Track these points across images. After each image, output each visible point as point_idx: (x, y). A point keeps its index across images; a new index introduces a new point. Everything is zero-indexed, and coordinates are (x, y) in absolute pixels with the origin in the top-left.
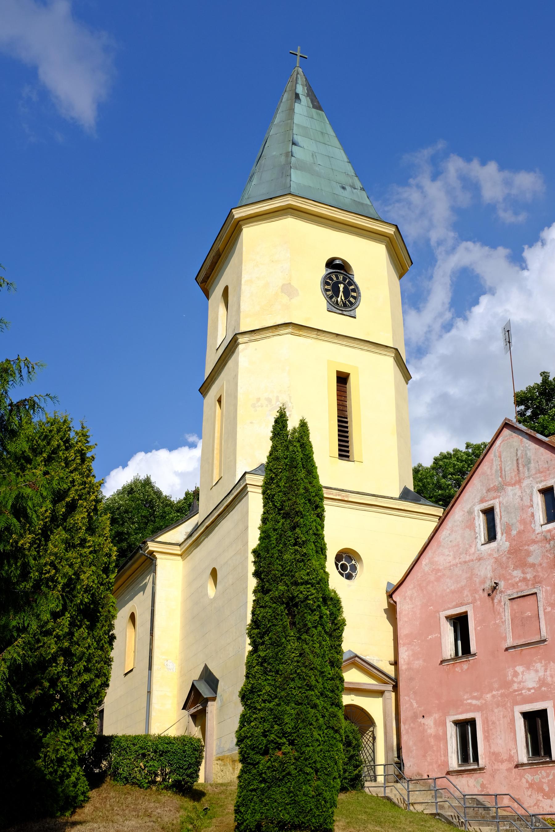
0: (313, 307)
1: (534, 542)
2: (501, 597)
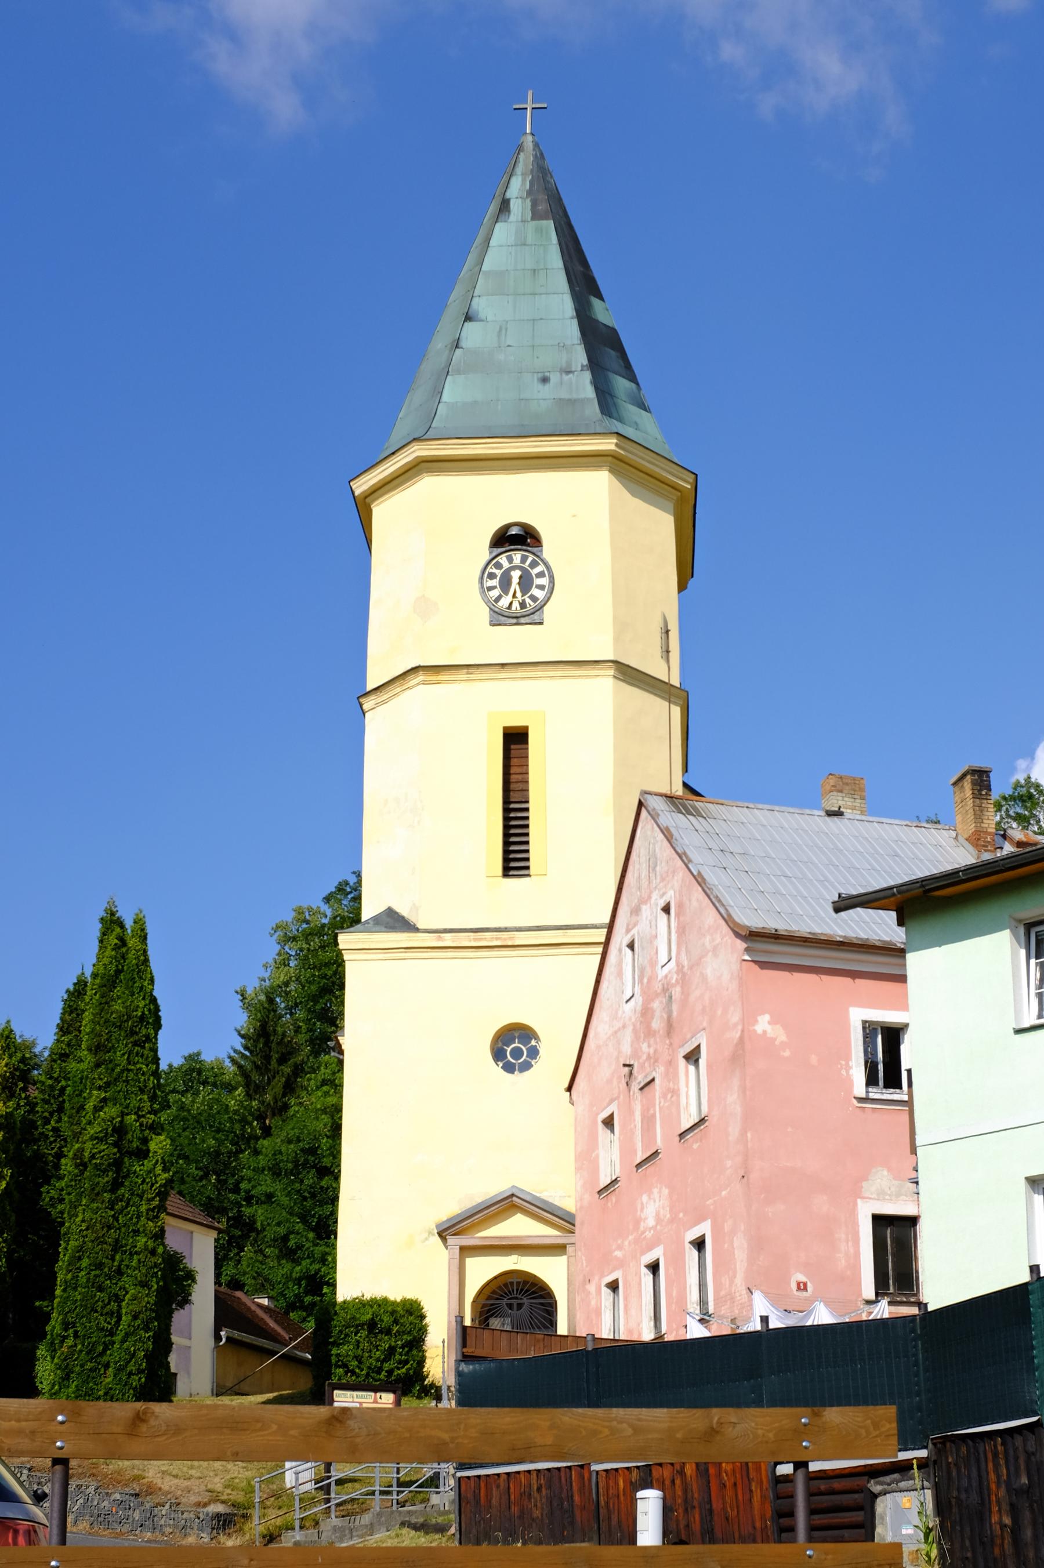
0: (466, 629)
1: (657, 995)
2: (635, 1086)
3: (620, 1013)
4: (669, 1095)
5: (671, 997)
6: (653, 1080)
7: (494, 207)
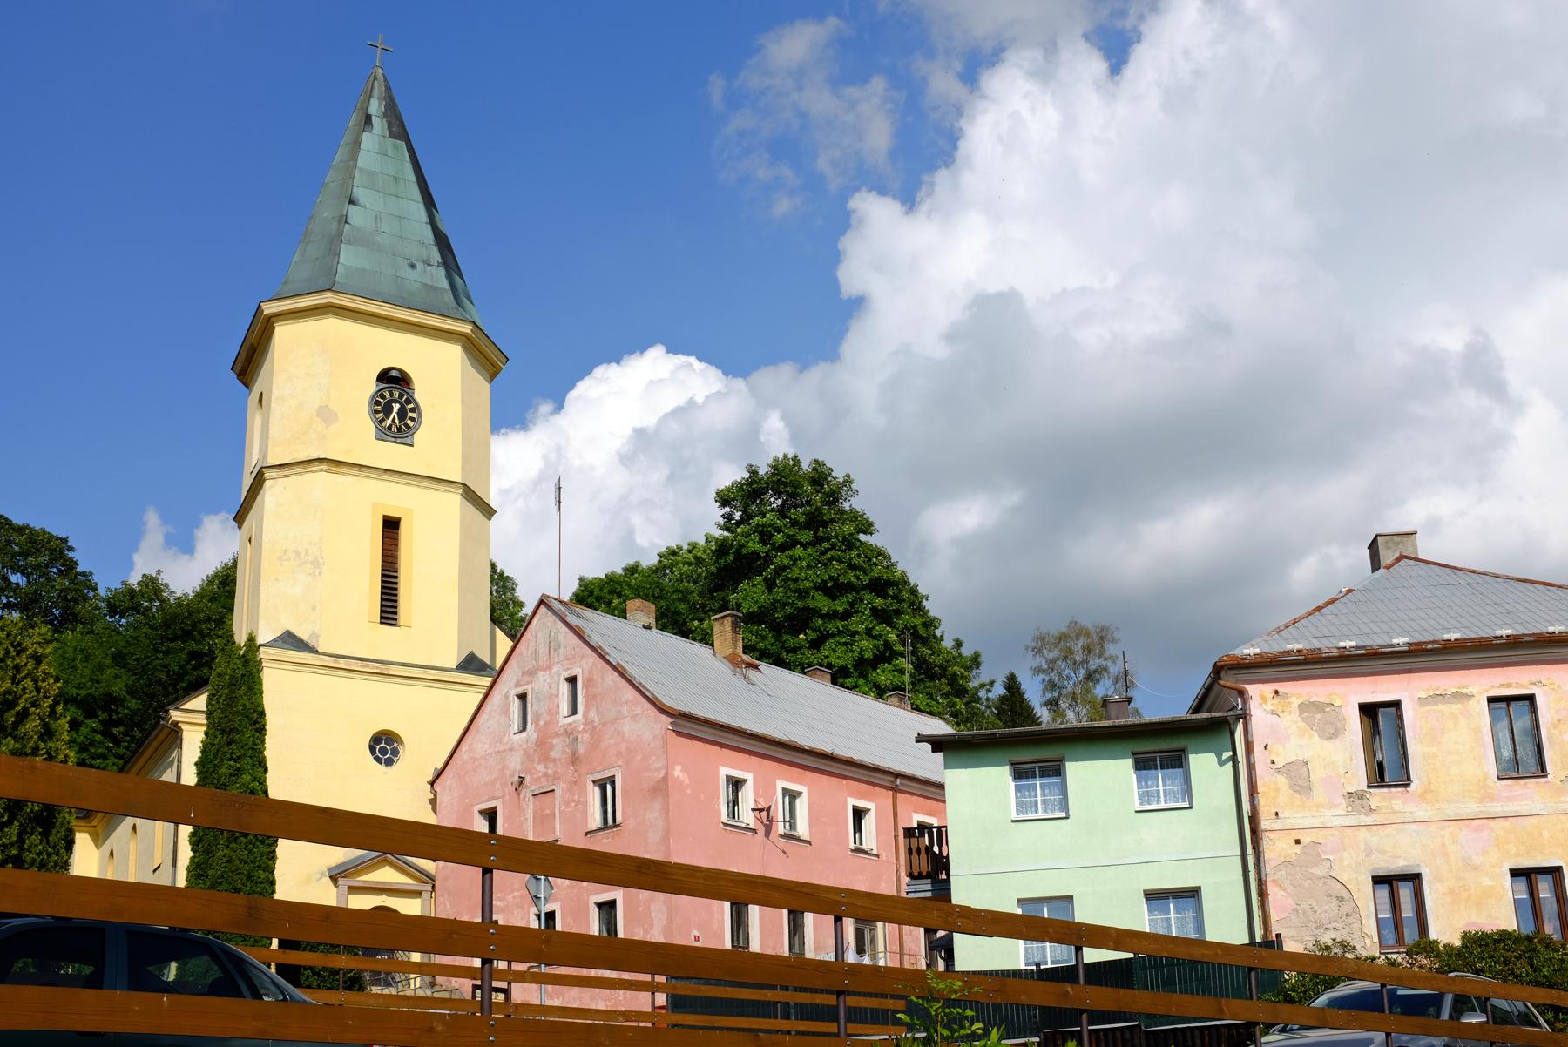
0: (356, 434)
1: (557, 735)
2: (526, 793)
7: (354, 118)
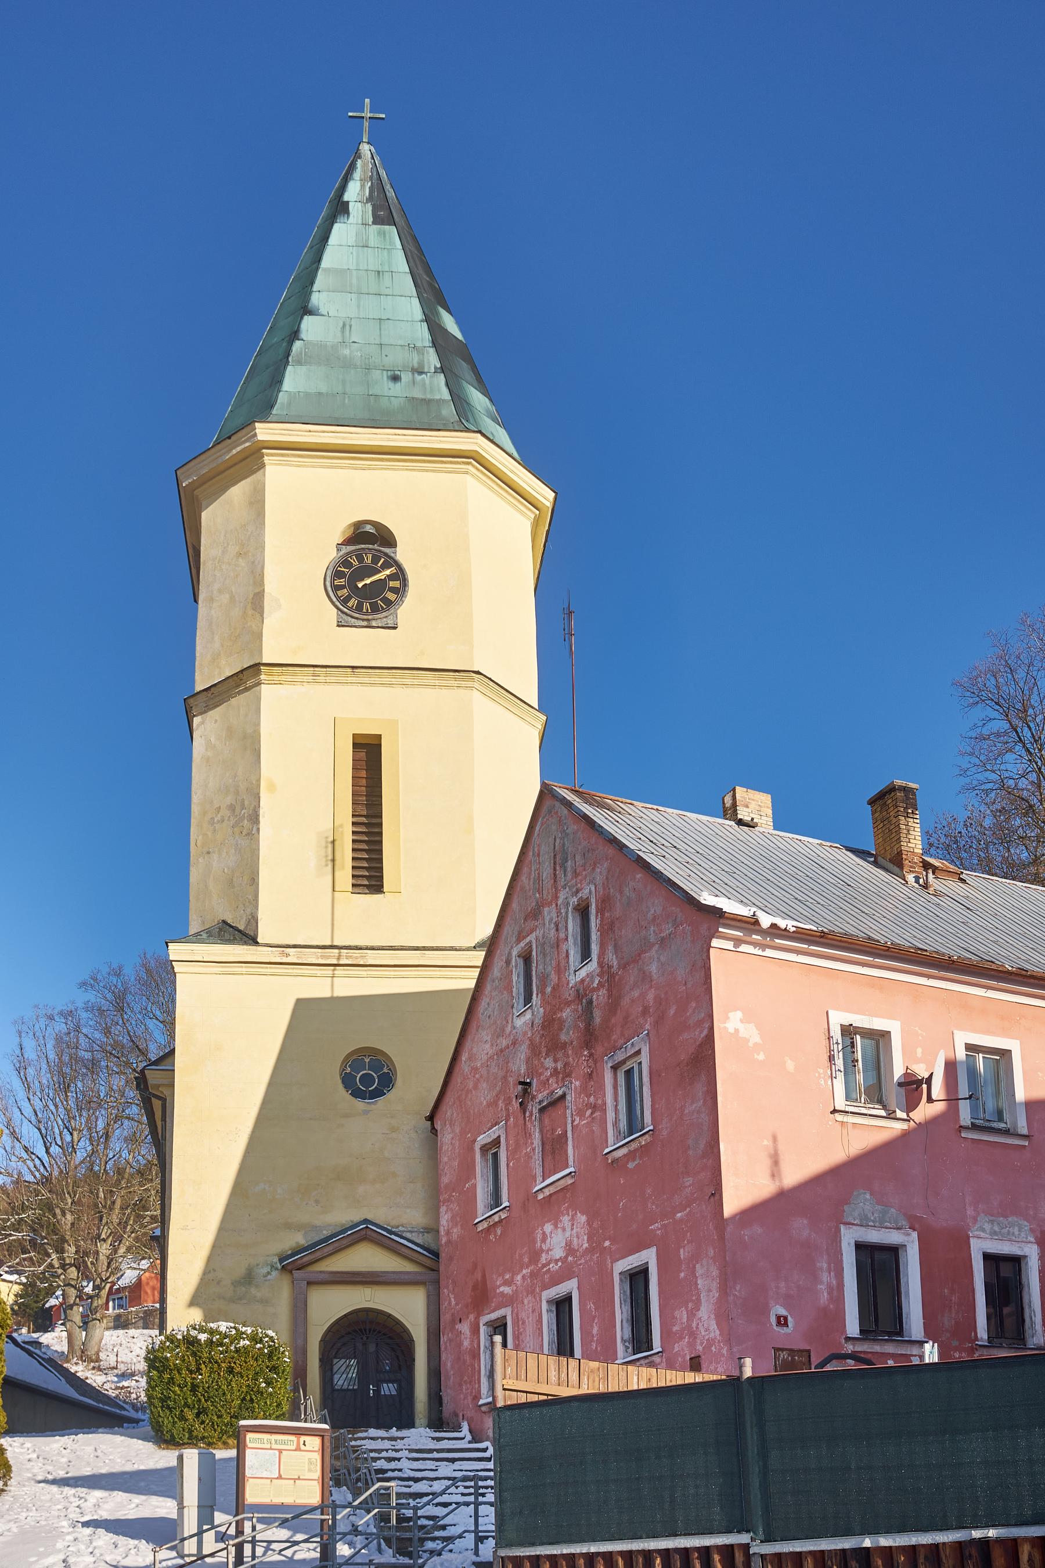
1: (568, 1004)
2: (534, 1108)
3: (508, 1029)
4: (589, 1112)
5: (590, 1002)
6: (563, 1097)
